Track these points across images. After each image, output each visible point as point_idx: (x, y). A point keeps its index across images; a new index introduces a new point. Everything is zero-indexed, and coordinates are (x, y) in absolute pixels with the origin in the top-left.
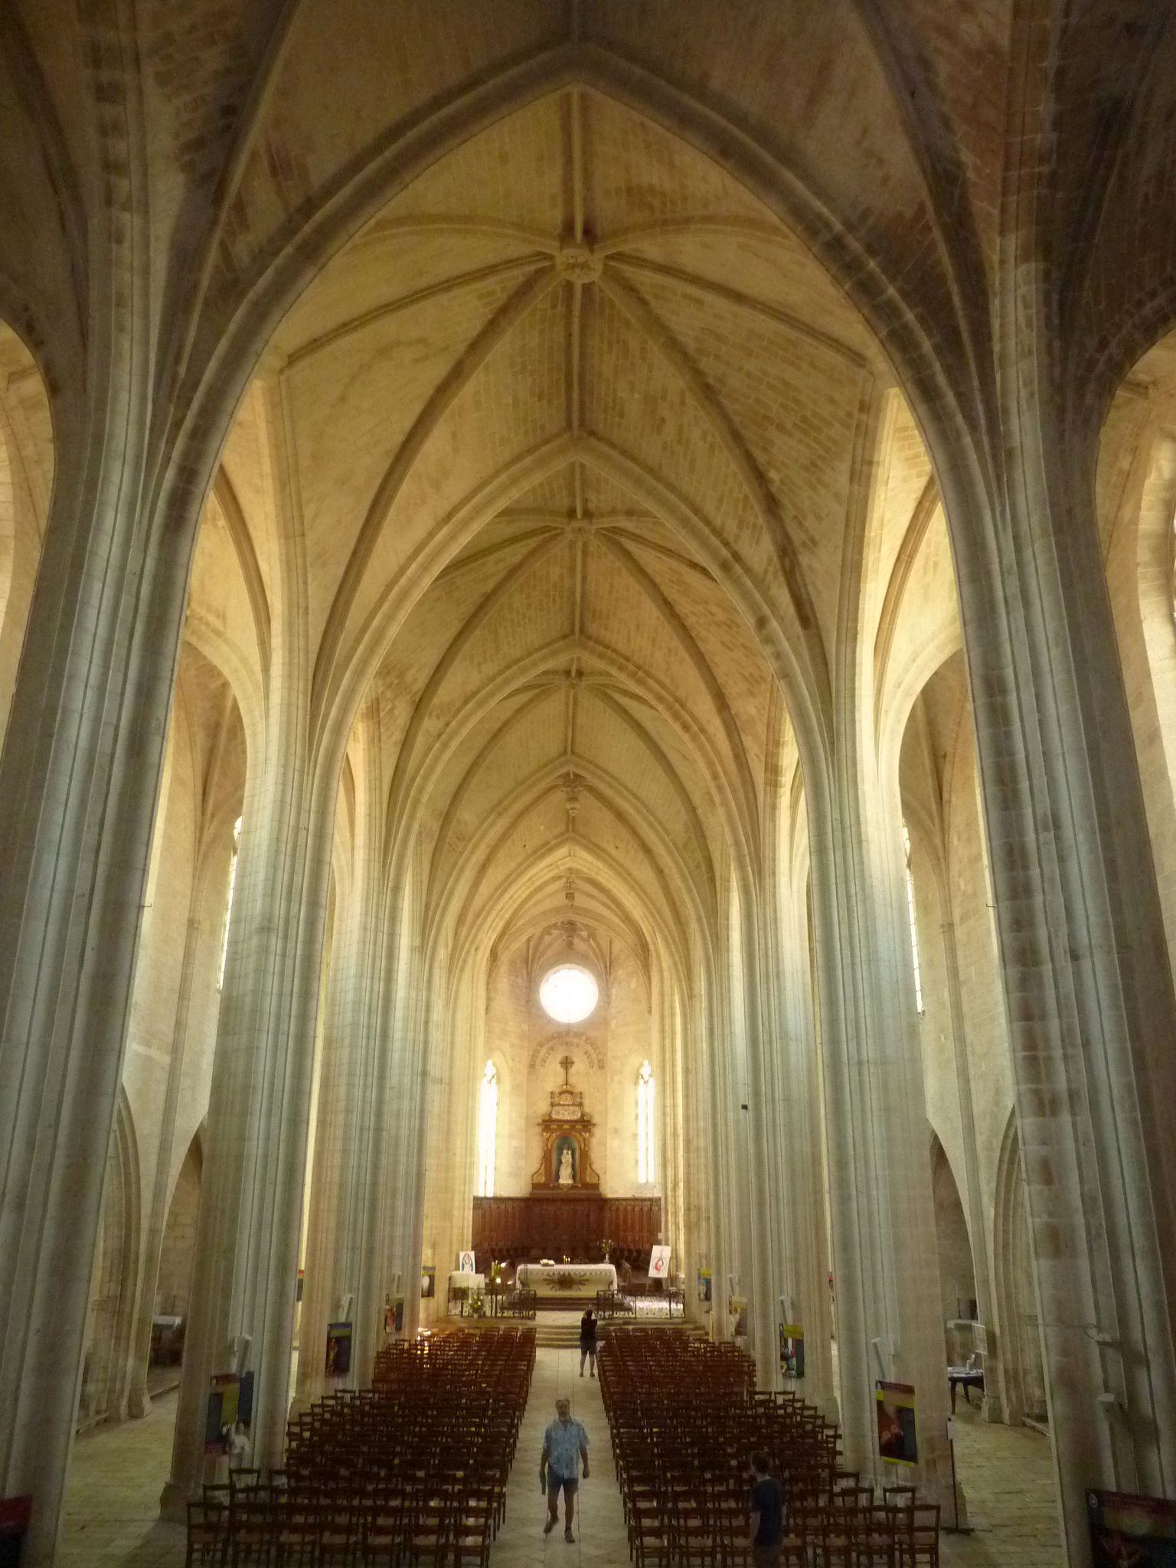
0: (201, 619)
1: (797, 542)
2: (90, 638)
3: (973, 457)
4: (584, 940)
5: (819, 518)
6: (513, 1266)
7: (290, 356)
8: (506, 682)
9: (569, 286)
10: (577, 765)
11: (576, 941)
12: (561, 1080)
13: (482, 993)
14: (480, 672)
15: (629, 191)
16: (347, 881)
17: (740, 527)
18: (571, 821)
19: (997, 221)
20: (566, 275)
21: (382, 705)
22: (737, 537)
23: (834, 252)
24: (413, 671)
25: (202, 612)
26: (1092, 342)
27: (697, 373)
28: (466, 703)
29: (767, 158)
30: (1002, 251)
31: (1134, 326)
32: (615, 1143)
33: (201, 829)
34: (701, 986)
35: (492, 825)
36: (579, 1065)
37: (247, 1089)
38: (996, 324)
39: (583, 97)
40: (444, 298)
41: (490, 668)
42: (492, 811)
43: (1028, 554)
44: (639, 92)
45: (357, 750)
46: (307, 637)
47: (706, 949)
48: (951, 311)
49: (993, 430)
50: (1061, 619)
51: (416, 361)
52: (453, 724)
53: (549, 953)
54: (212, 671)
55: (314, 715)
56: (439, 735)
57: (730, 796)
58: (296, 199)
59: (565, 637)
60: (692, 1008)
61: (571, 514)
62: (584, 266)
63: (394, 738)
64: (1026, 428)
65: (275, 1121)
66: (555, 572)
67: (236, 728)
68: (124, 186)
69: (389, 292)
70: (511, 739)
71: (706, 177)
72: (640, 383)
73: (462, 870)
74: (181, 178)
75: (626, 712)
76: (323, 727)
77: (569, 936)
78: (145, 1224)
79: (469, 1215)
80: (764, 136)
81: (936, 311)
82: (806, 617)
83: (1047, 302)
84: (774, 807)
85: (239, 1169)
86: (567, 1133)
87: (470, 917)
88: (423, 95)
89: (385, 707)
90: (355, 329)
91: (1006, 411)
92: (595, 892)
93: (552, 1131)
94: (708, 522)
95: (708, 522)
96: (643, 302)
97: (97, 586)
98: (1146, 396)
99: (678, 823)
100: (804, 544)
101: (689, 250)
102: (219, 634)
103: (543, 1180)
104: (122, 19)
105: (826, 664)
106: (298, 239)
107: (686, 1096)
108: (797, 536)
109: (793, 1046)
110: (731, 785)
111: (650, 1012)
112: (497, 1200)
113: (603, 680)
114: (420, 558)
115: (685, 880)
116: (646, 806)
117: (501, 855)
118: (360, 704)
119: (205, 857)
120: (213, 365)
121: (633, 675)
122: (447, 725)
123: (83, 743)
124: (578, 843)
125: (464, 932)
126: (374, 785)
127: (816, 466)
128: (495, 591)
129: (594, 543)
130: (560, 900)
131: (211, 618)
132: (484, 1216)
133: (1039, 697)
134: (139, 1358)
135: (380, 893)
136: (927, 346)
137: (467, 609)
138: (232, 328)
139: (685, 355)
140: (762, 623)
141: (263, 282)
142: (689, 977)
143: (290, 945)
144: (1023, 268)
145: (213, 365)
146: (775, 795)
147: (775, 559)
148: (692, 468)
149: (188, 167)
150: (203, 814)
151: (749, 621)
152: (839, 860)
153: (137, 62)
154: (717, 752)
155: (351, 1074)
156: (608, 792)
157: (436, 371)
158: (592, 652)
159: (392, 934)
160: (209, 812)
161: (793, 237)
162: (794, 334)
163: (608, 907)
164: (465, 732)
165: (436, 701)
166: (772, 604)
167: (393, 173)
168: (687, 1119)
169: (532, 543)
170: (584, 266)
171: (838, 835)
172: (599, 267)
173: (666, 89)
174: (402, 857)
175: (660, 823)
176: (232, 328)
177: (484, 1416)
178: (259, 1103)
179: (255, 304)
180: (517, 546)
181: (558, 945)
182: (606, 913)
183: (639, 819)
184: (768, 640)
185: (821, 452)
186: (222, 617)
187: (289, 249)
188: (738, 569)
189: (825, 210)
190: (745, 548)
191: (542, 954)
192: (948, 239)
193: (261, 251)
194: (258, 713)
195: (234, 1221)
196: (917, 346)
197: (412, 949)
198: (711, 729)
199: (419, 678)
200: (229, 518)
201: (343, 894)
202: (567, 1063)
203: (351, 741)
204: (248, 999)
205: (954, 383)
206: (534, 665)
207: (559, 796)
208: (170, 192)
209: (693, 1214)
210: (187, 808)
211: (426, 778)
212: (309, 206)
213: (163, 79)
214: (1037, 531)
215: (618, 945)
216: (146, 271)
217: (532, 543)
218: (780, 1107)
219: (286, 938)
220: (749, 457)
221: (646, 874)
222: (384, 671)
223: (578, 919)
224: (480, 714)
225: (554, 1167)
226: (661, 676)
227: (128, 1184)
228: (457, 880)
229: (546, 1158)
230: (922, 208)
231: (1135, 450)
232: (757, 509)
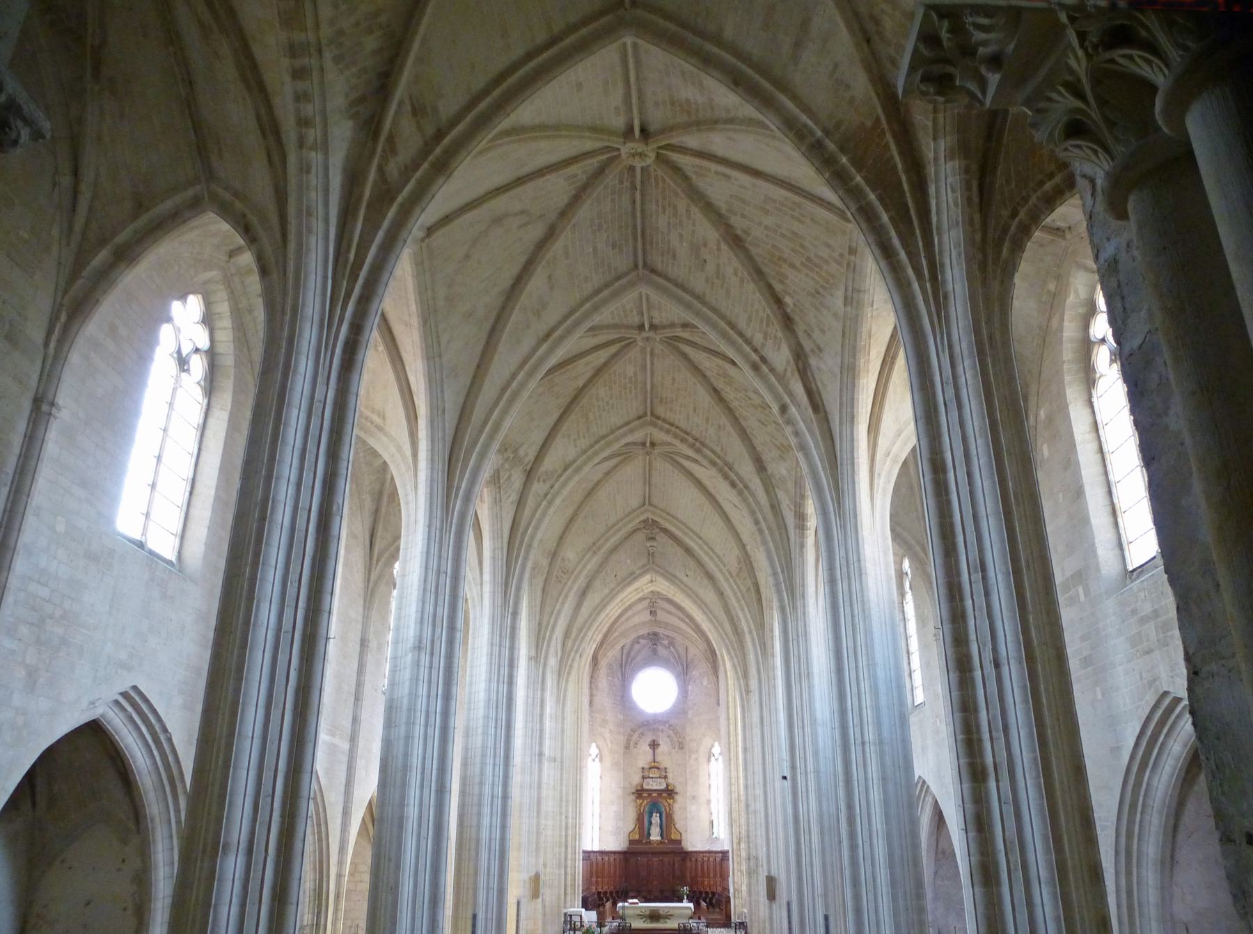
0: (367, 418)
2: (290, 448)
3: (920, 299)
4: (665, 647)
5: (823, 332)
6: (614, 904)
8: (596, 454)
9: (632, 169)
10: (653, 513)
11: (659, 648)
12: (650, 758)
13: (586, 691)
14: (576, 446)
15: (673, 103)
16: (478, 609)
17: (765, 338)
18: (651, 555)
19: (931, 131)
20: (630, 162)
21: (502, 474)
22: (763, 345)
23: (816, 151)
24: (524, 447)
25: (367, 413)
26: (1005, 213)
27: (728, 227)
28: (565, 470)
29: (766, 84)
30: (935, 152)
31: (1038, 199)
32: (694, 808)
33: (369, 570)
34: (755, 697)
35: (589, 560)
36: (664, 747)
37: (406, 768)
38: (933, 202)
39: (635, 46)
40: (540, 182)
41: (584, 443)
42: (589, 549)
43: (960, 369)
44: (673, 42)
45: (483, 509)
46: (444, 431)
47: (756, 655)
50: (983, 418)
51: (520, 227)
52: (556, 486)
53: (639, 658)
54: (375, 454)
56: (546, 495)
57: (769, 538)
58: (430, 130)
59: (639, 418)
60: (748, 701)
61: (641, 327)
62: (641, 155)
63: (511, 499)
64: (955, 278)
65: (426, 791)
66: (630, 370)
67: (394, 494)
68: (312, 134)
69: (499, 180)
70: (602, 494)
71: (727, 99)
72: (685, 234)
73: (566, 596)
74: (350, 124)
75: (691, 474)
76: (456, 496)
77: (656, 645)
79: (580, 865)
80: (764, 71)
82: (816, 404)
83: (968, 187)
84: (802, 546)
85: (401, 827)
86: (654, 800)
87: (575, 631)
88: (518, 52)
89: (504, 476)
90: (475, 207)
91: (942, 265)
92: (673, 610)
93: (644, 798)
94: (741, 335)
95: (741, 335)
96: (686, 178)
97: (295, 412)
98: (1063, 237)
99: (732, 556)
100: (813, 351)
101: (718, 142)
102: (380, 429)
103: (637, 837)
104: (310, 23)
105: (832, 440)
106: (431, 158)
107: (746, 770)
108: (807, 345)
109: (820, 729)
110: (769, 529)
111: (718, 704)
112: (601, 853)
113: (667, 449)
114: (527, 368)
115: (738, 601)
116: (706, 544)
117: (597, 583)
118: (486, 473)
119: (373, 591)
120: (373, 250)
121: (692, 446)
122: (552, 487)
124: (657, 572)
125: (570, 643)
126: (496, 536)
127: (818, 293)
128: (585, 386)
129: (659, 348)
130: (646, 616)
131: (375, 418)
132: (591, 865)
133: (970, 475)
135: (503, 617)
136: (885, 218)
137: (564, 401)
138: (386, 224)
139: (720, 215)
140: (783, 409)
141: (406, 192)
142: (746, 677)
143: (435, 659)
144: (950, 164)
145: (373, 250)
146: (802, 536)
147: (792, 362)
148: (728, 292)
149: (354, 116)
150: (371, 559)
151: (775, 409)
152: (846, 587)
153: (320, 51)
154: (758, 503)
155: (484, 756)
156: (678, 533)
157: (536, 232)
158: (661, 429)
159: (512, 648)
160: (375, 558)
161: (787, 140)
162: (797, 199)
163: (682, 620)
164: (565, 492)
165: (542, 469)
166: (791, 394)
167: (500, 106)
168: (746, 787)
169: (613, 349)
170: (641, 155)
171: (844, 569)
172: (653, 155)
173: (693, 40)
174: (519, 589)
175: (718, 557)
176: (386, 224)
178: (414, 778)
180: (601, 352)
182: (683, 626)
183: (701, 553)
184: (789, 422)
185: (822, 282)
187: (426, 165)
188: (764, 368)
189: (809, 122)
190: (770, 353)
191: (633, 659)
192: (898, 143)
193: (406, 167)
194: (410, 487)
195: (398, 867)
196: (878, 218)
197: (530, 659)
198: (751, 485)
200: (387, 346)
201: (475, 618)
202: (654, 745)
203: (478, 501)
204: (405, 701)
205: (905, 245)
206: (617, 439)
207: (640, 536)
208: (342, 133)
209: (752, 862)
210: (359, 556)
211: (537, 528)
212: (439, 135)
213: (337, 59)
214: (966, 353)
215: (693, 651)
216: (326, 191)
217: (613, 349)
218: (811, 777)
219: (432, 654)
220: (770, 287)
221: (710, 596)
222: (503, 449)
223: (660, 631)
224: (576, 478)
225: (646, 824)
227: (320, 840)
228: (563, 604)
229: (640, 819)
230: (878, 120)
231: (1058, 278)
232: (777, 326)
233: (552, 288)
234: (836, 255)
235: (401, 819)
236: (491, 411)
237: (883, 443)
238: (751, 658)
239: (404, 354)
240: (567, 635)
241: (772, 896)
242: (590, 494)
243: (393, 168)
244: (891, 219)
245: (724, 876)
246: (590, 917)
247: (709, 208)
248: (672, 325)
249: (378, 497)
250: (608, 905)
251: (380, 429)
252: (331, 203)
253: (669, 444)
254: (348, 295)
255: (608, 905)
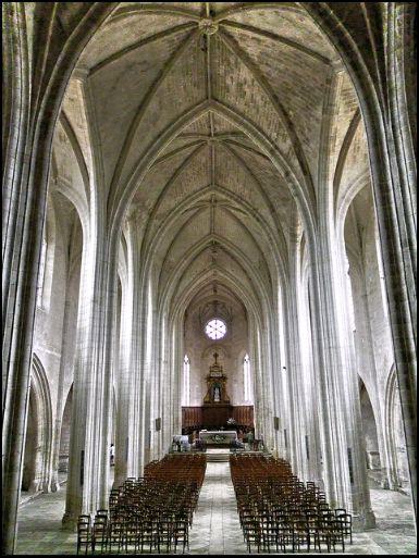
1: (301, 141)
5: (310, 130)
6: (198, 433)
7: (91, 70)
12: (213, 362)
18: (214, 260)
33: (68, 266)
36: (220, 357)
38: (385, 34)
48: (366, 31)
49: (384, 81)
54: (71, 204)
55: (108, 218)
61: (210, 135)
62: (210, 27)
78: (54, 418)
81: (359, 32)
84: (294, 250)
85: (86, 394)
87: (122, 178)
91: (389, 72)
94: (263, 133)
95: (263, 133)
96: (236, 42)
102: (70, 187)
105: (314, 188)
118: (127, 213)
121: (236, 200)
123: (10, 223)
134: (54, 469)
136: (355, 47)
140: (287, 174)
158: (220, 191)
166: (292, 166)
172: (217, 27)
174: (147, 274)
177: (309, 543)
179: (72, 42)
181: (211, 311)
186: (70, 180)
197: (153, 312)
199: (150, 203)
202: (216, 356)
207: (209, 251)
217: (194, 147)
220: (281, 106)
226: (247, 199)
229: (209, 392)
233: (161, 109)
234: (318, 85)
235: (87, 390)
236: (129, 176)
237: (341, 191)
238: (266, 310)
239: (81, 145)
240: (172, 301)
241: (277, 427)
242: (182, 229)
243: (65, 19)
244: (359, 47)
245: (251, 418)
246: (186, 438)
247: (247, 59)
248: (227, 133)
249: (71, 227)
250: (195, 433)
251: (70, 187)
252: (83, 146)
253: (226, 200)
254: (42, 94)
255: (195, 433)
